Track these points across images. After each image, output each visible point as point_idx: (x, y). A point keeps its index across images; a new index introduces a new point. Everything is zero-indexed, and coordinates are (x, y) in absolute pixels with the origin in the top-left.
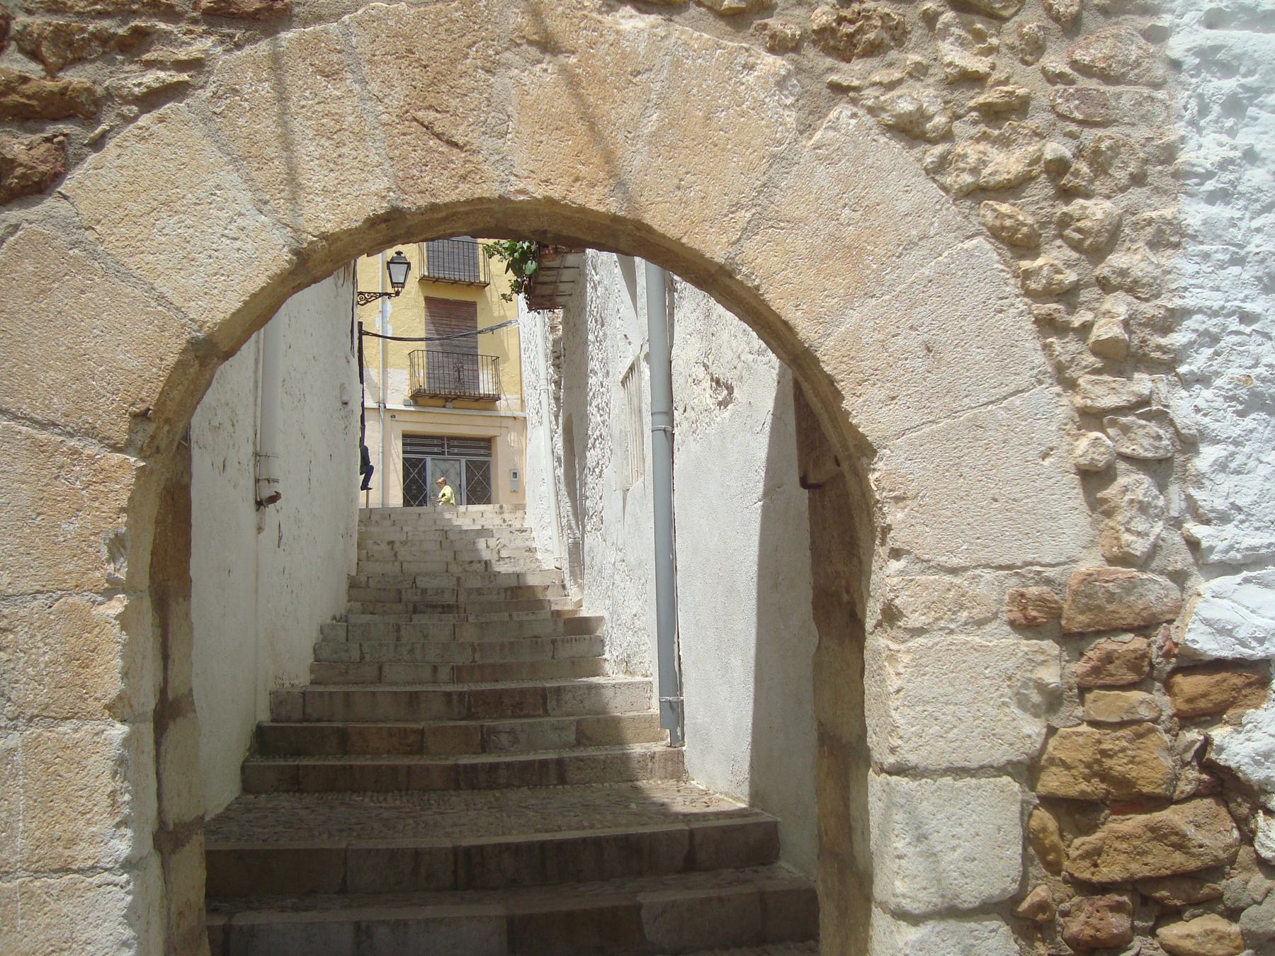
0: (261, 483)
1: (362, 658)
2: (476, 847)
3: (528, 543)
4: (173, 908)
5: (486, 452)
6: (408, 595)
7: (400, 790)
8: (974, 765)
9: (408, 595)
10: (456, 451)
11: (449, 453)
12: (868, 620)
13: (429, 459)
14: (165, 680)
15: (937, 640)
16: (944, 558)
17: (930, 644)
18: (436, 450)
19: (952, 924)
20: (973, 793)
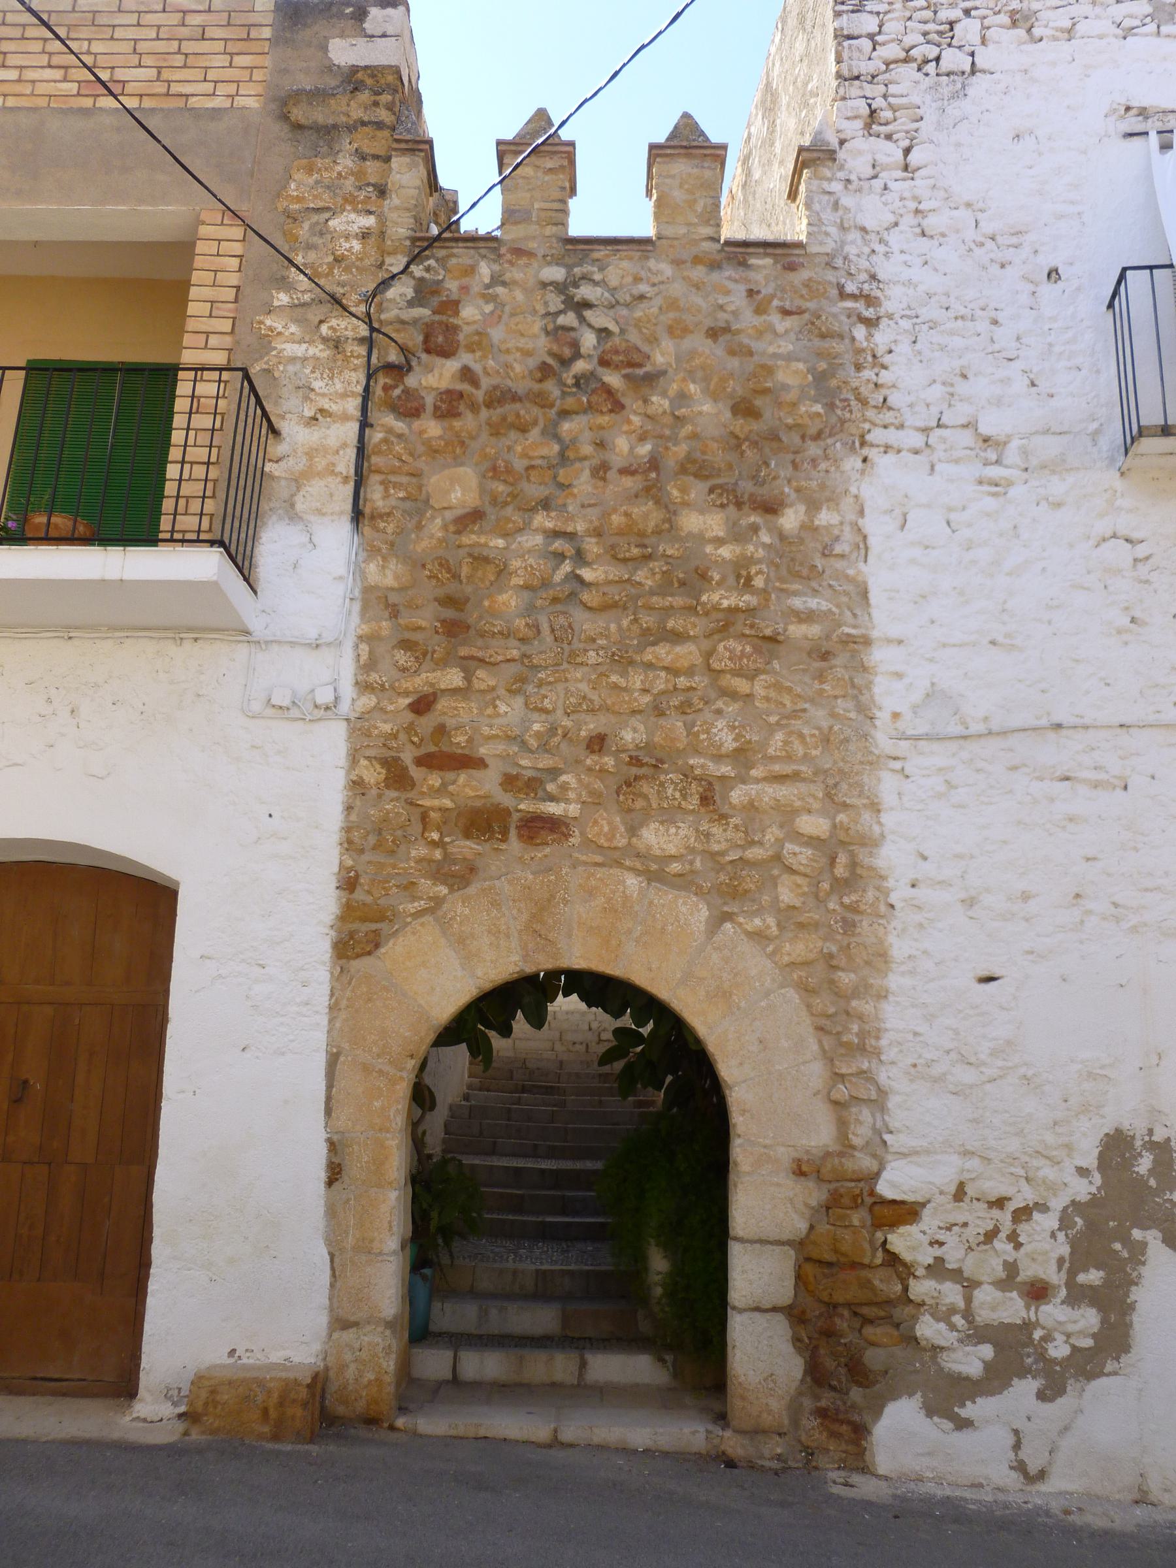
19: (757, 1315)
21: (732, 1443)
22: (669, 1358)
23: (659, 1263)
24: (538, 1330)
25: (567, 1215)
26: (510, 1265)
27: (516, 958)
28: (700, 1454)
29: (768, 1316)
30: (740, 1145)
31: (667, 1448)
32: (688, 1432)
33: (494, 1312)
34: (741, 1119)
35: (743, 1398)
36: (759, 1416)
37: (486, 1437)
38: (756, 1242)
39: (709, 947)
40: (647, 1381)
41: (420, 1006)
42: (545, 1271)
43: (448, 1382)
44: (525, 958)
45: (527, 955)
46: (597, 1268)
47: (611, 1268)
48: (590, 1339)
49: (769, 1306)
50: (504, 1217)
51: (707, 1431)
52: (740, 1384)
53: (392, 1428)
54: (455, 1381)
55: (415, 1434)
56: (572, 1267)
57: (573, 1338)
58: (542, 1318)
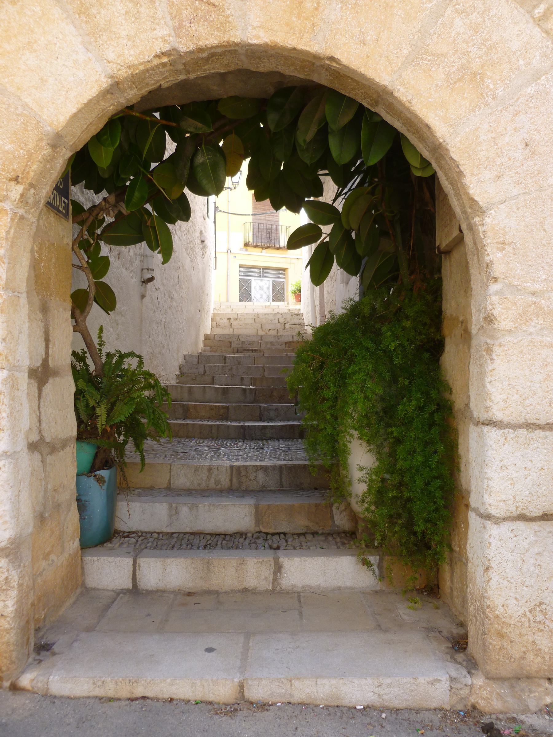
0: (144, 271)
1: (205, 372)
2: (243, 466)
3: (301, 321)
4: (49, 487)
5: (282, 276)
6: (234, 345)
7: (213, 438)
8: (542, 422)
9: (234, 345)
10: (267, 275)
11: (263, 277)
12: (473, 327)
13: (253, 279)
14: (47, 353)
15: (520, 338)
16: (529, 284)
17: (516, 341)
18: (257, 274)
19: (521, 525)
20: (541, 441)
21: (485, 694)
22: (373, 559)
23: (361, 459)
24: (231, 527)
25: (264, 421)
26: (207, 463)
27: (163, 31)
28: (441, 709)
29: (536, 526)
30: (497, 293)
31: (396, 704)
32: (421, 679)
33: (184, 510)
34: (499, 255)
35: (501, 635)
36: (523, 658)
37: (144, 698)
38: (520, 426)
39: (449, 10)
40: (349, 584)
41: (25, 106)
42: (239, 467)
43: (128, 590)
44: (179, 29)
45: (181, 27)
46: (290, 463)
47: (306, 462)
48: (285, 534)
49: (538, 513)
50: (212, 423)
51: (452, 679)
52: (497, 617)
53: (15, 688)
54: (135, 591)
55: (50, 698)
56: (267, 463)
57: (267, 534)
58: (235, 515)
